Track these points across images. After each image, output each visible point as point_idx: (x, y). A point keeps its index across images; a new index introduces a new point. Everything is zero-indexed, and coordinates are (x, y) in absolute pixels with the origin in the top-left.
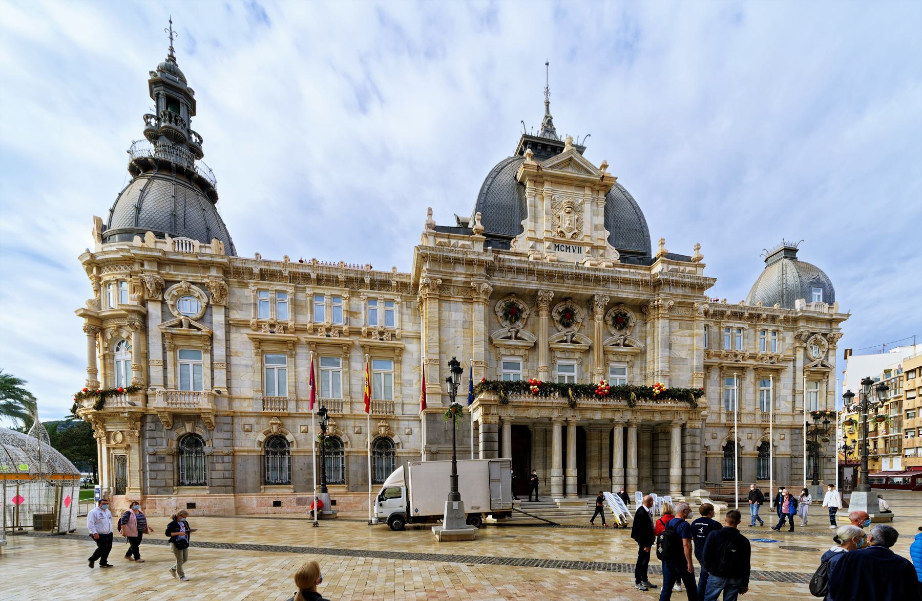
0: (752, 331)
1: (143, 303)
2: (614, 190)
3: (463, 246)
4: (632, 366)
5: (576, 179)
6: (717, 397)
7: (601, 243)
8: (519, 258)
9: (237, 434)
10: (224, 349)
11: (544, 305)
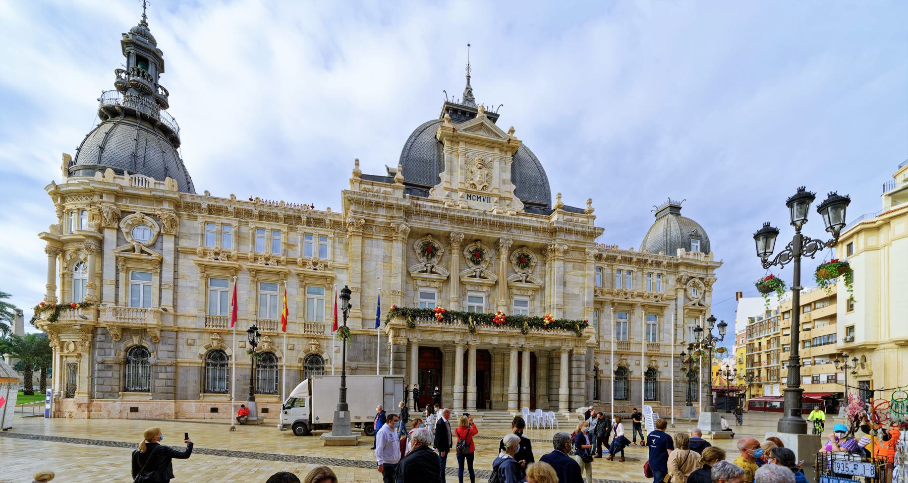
0: (640, 274)
1: (101, 230)
2: (520, 150)
3: (385, 193)
4: (533, 300)
5: (486, 141)
8: (435, 205)
9: (180, 347)
10: (172, 273)
11: (455, 245)
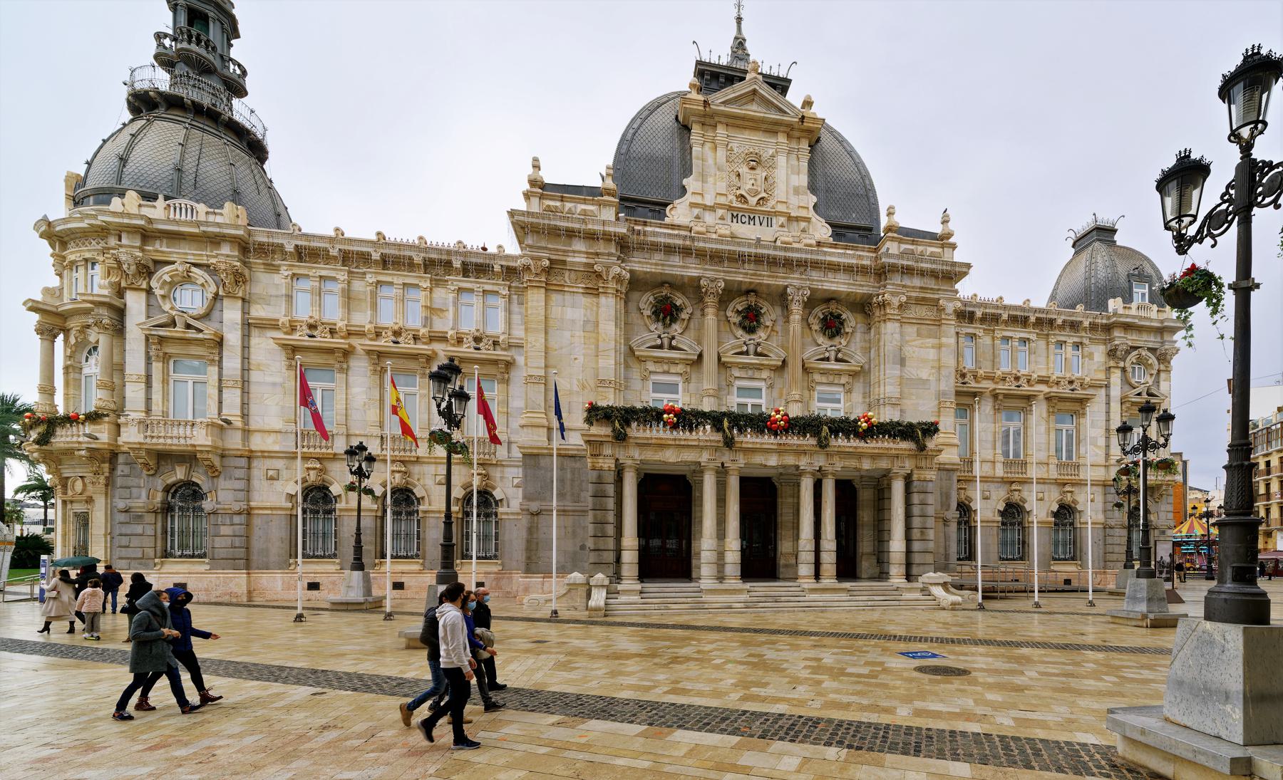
0: (1042, 343)
3: (584, 212)
4: (849, 391)
6: (990, 438)
7: (803, 213)
8: (676, 232)
9: (256, 483)
10: (239, 361)
11: (710, 300)
